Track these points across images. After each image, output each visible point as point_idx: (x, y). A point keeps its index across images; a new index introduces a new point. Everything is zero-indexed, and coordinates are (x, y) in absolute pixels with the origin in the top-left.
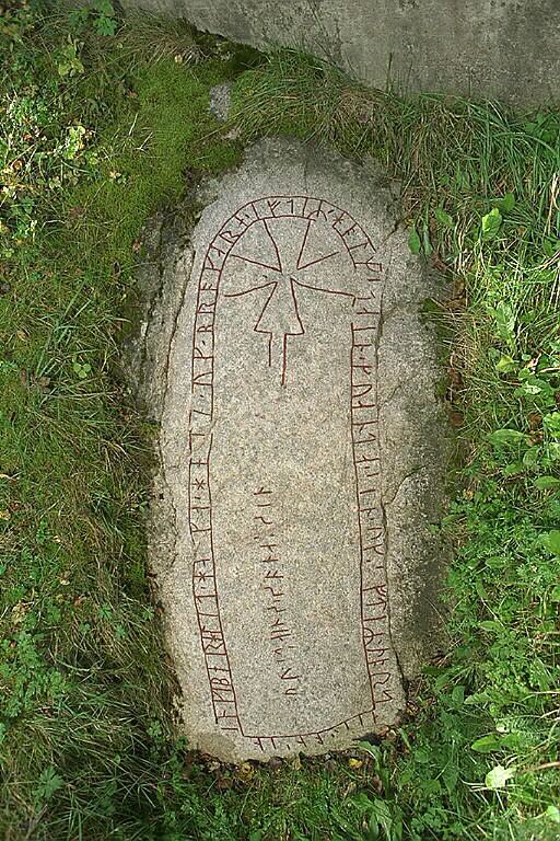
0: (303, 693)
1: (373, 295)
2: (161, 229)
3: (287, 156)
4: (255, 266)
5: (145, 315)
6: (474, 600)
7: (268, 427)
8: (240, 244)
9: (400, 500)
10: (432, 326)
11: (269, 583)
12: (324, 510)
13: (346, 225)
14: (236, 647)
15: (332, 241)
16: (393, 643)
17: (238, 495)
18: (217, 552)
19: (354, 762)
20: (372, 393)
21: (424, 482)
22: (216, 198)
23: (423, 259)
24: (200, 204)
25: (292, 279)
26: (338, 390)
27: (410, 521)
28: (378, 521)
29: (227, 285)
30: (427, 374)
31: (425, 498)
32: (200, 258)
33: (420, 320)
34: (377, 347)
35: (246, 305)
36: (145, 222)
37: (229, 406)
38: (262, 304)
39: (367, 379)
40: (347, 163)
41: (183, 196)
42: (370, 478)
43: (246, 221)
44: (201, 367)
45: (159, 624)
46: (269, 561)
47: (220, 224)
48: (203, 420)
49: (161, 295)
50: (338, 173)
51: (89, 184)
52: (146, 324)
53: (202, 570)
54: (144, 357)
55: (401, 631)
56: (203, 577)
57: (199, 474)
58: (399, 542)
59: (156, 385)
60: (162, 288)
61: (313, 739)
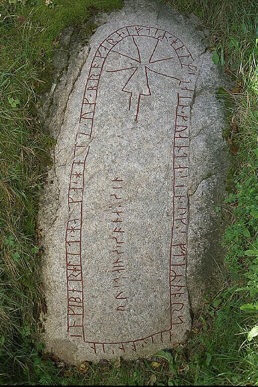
0: (129, 310)
1: (191, 81)
2: (71, 35)
3: (148, 8)
4: (126, 58)
5: (55, 80)
6: (243, 238)
7: (125, 143)
8: (117, 46)
9: (200, 191)
10: (223, 101)
11: (115, 235)
12: (154, 193)
13: (179, 44)
14: (90, 275)
15: (170, 51)
16: (187, 283)
17: (101, 182)
18: (84, 214)
19: (156, 364)
20: (187, 131)
21: (214, 182)
22: (105, 23)
23: (219, 67)
24: (96, 25)
25: (146, 67)
26: (168, 127)
27: (204, 205)
28: (185, 204)
29: (108, 66)
30: (218, 126)
31: (214, 192)
32: (93, 51)
33: (216, 97)
34: (191, 108)
35: (119, 79)
36: (62, 31)
37: (102, 130)
38: (128, 77)
39: (184, 123)
40: (181, 16)
41: (86, 21)
42: (182, 179)
43: (122, 35)
44: (87, 109)
45: (39, 258)
46: (116, 221)
47: (108, 35)
48: (85, 138)
49: (67, 69)
50: (175, 20)
51: (32, 6)
52: (55, 85)
53: (74, 225)
54: (51, 103)
55: (193, 275)
56: (73, 229)
57: (78, 169)
58: (197, 218)
59: (57, 118)
60: (68, 66)
61: (129, 346)
